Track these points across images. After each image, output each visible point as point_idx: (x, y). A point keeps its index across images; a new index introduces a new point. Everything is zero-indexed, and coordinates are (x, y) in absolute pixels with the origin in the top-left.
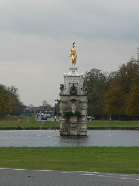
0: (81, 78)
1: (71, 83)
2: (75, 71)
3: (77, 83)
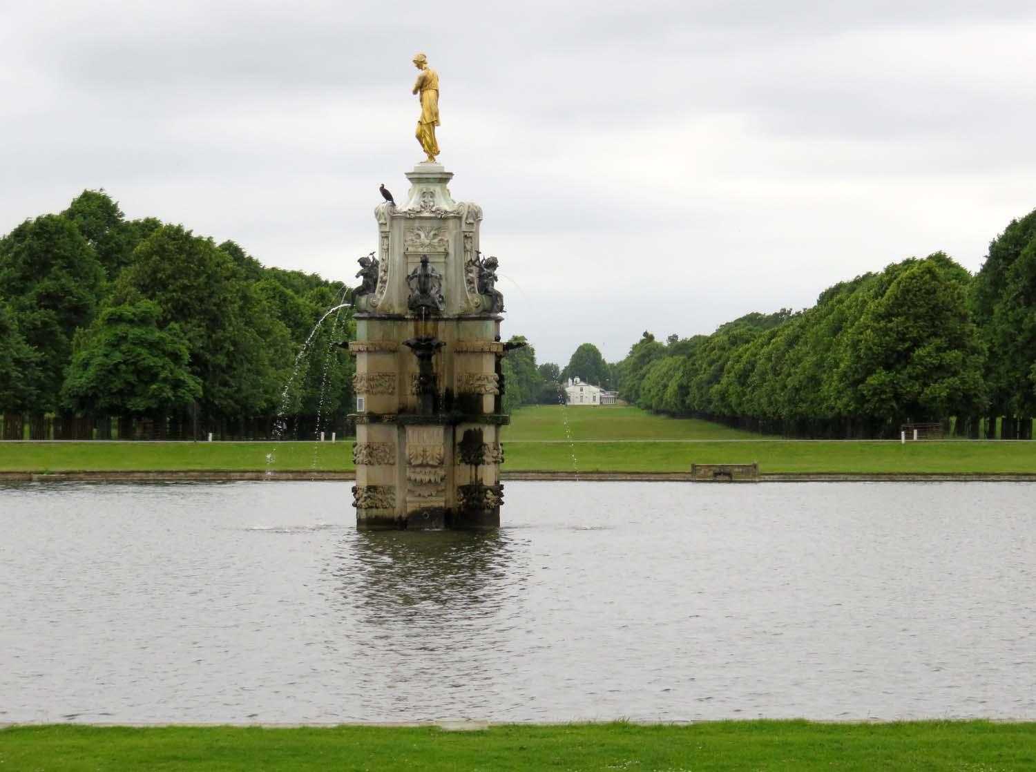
0: (464, 227)
1: (415, 255)
2: (437, 188)
3: (447, 254)
